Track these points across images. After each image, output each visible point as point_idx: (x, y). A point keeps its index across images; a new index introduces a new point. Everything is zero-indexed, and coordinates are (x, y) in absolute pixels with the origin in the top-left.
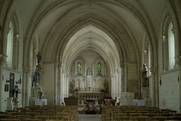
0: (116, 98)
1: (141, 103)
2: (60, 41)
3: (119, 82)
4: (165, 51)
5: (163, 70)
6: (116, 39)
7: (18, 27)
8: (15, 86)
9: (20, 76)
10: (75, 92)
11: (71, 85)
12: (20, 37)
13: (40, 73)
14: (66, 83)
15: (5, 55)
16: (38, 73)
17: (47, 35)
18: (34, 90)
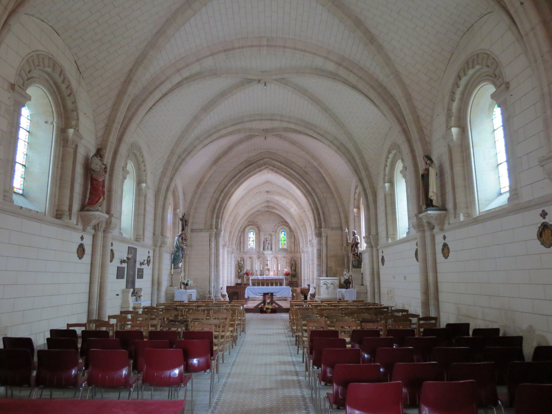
0: (309, 285)
1: (349, 295)
2: (219, 195)
3: (313, 260)
4: (389, 208)
5: (387, 240)
6: (308, 191)
7: (144, 171)
8: (138, 269)
9: (149, 253)
10: (245, 276)
11: (240, 267)
12: (147, 187)
13: (185, 247)
14: (231, 263)
15: (114, 215)
16: (181, 247)
17: (198, 186)
18: (173, 276)
